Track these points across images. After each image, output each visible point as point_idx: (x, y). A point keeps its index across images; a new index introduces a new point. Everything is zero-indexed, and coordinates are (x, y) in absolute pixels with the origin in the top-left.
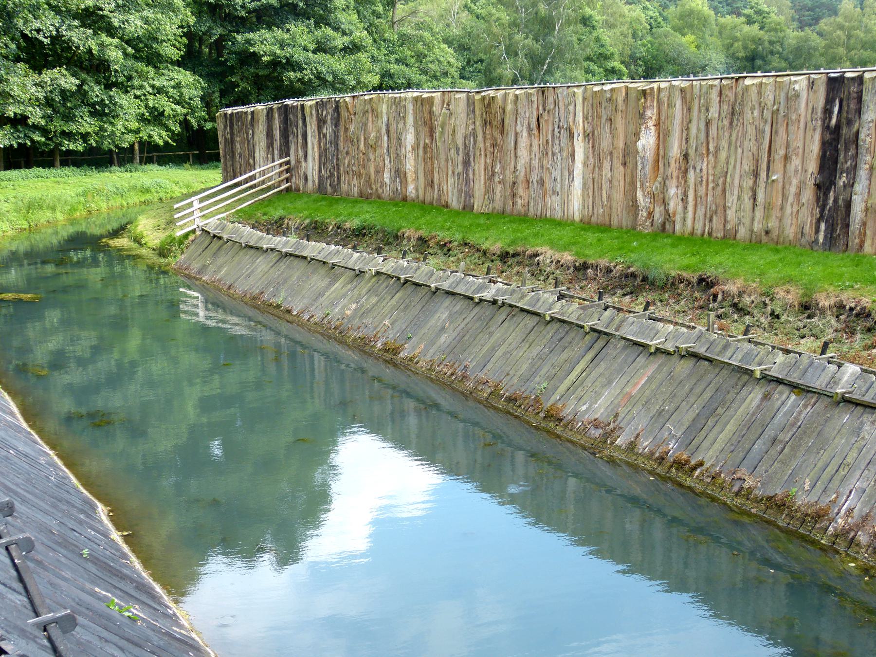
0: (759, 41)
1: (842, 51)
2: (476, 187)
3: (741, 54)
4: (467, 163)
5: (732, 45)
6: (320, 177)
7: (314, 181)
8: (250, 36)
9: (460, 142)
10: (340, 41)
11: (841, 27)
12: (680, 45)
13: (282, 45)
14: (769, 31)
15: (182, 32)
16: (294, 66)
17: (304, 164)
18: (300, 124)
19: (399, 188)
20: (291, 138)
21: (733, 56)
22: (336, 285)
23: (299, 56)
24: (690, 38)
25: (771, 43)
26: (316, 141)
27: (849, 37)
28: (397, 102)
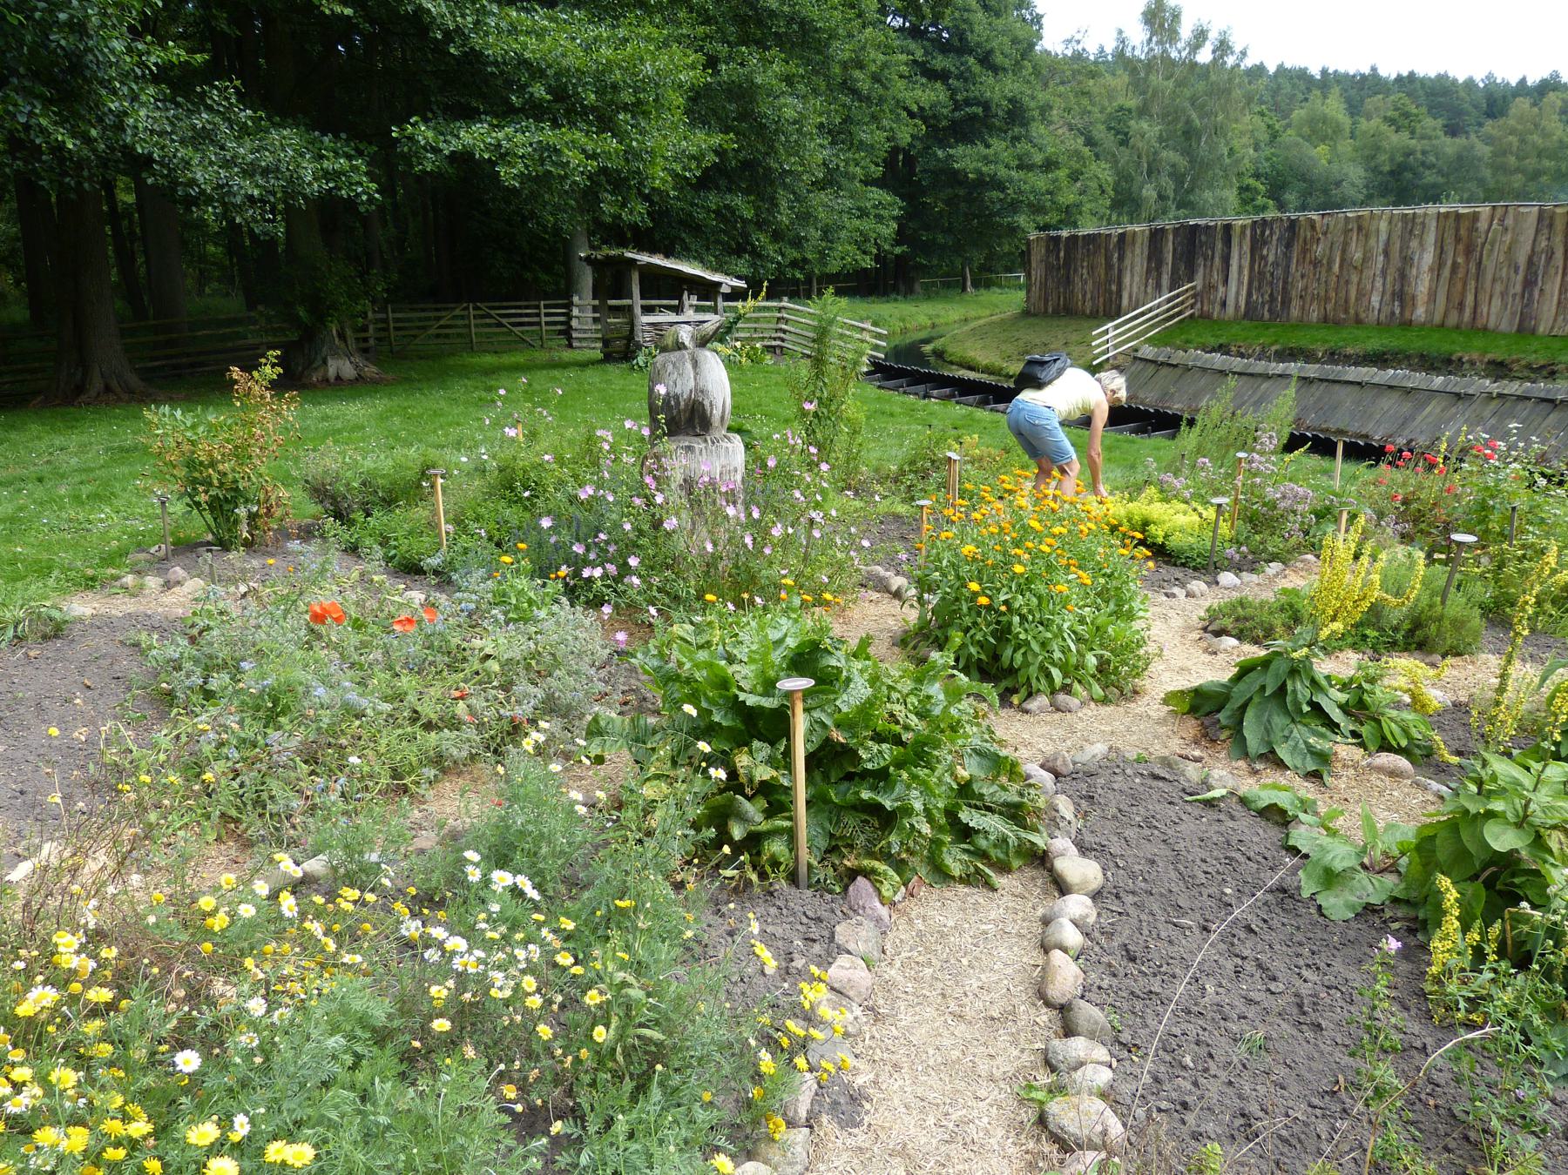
0: (1409, 153)
1: (1512, 160)
2: (1545, 308)
3: (1387, 168)
4: (1529, 283)
5: (1373, 157)
6: (1248, 303)
7: (1237, 307)
8: (951, 151)
9: (1522, 260)
10: (1038, 158)
11: (1513, 132)
12: (1311, 158)
13: (986, 160)
14: (1423, 137)
15: (988, 146)
16: (1000, 185)
17: (1221, 289)
18: (1219, 245)
19: (1397, 312)
20: (1201, 261)
21: (1375, 170)
22: (1428, 409)
23: (1002, 172)
24: (1322, 149)
25: (1424, 153)
26: (1246, 263)
27: (1523, 141)
28: (1409, 222)
